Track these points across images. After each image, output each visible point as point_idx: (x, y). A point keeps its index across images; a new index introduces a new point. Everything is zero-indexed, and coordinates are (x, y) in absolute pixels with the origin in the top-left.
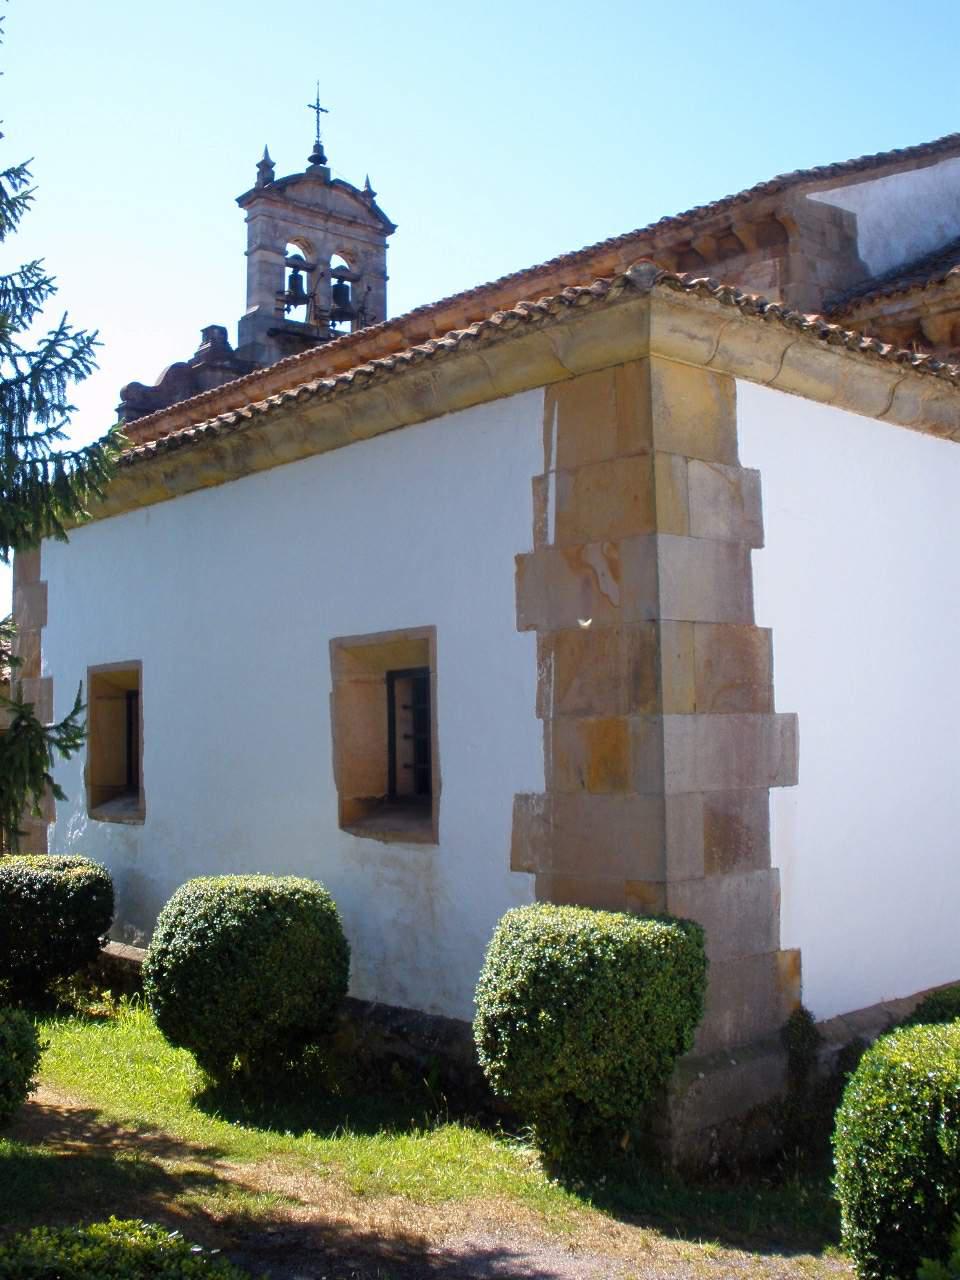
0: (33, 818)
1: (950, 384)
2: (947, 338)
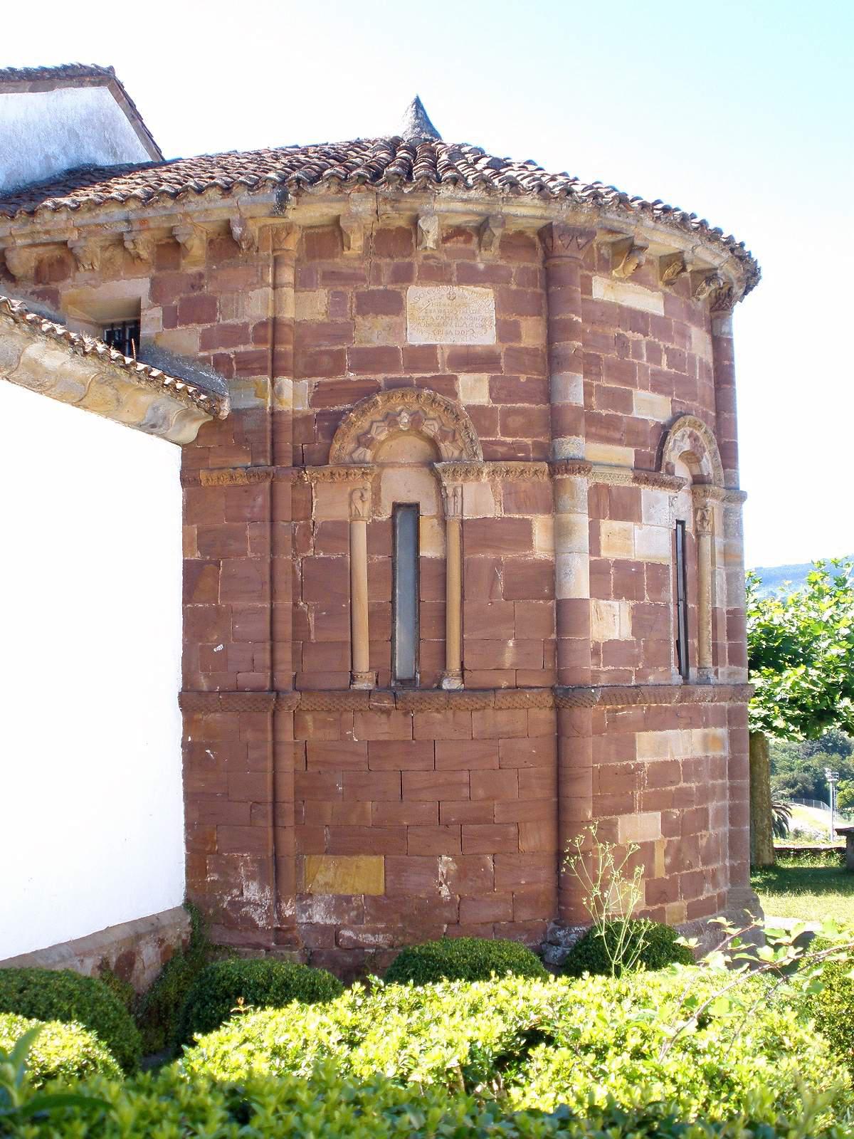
0: (824, 763)
1: (11, 320)
2: (31, 273)
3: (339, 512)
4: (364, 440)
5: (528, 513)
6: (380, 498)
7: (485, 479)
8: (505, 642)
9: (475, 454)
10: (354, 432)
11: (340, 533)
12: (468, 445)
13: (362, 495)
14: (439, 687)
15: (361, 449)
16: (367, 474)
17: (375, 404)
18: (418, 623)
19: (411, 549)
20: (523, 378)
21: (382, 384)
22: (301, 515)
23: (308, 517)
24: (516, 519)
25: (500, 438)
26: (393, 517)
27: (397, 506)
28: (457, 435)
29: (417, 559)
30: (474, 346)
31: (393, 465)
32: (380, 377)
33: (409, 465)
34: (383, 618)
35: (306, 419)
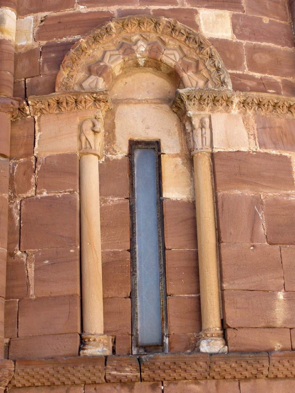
3: (68, 144)
4: (96, 69)
5: (285, 149)
6: (114, 136)
7: (235, 110)
8: (273, 294)
9: (223, 83)
10: (84, 60)
11: (69, 168)
12: (214, 74)
13: (94, 125)
14: (195, 348)
15: (93, 78)
16: (99, 100)
17: (108, 31)
18: (164, 274)
19: (153, 190)
20: (266, 20)
21: (116, 15)
22: (22, 152)
23: (28, 155)
24: (273, 155)
25: (247, 71)
26: (130, 155)
27: (134, 144)
28: (201, 66)
29: (160, 202)
31: (128, 101)
32: (114, 9)
33: (147, 101)
34: (121, 269)
35: (30, 53)
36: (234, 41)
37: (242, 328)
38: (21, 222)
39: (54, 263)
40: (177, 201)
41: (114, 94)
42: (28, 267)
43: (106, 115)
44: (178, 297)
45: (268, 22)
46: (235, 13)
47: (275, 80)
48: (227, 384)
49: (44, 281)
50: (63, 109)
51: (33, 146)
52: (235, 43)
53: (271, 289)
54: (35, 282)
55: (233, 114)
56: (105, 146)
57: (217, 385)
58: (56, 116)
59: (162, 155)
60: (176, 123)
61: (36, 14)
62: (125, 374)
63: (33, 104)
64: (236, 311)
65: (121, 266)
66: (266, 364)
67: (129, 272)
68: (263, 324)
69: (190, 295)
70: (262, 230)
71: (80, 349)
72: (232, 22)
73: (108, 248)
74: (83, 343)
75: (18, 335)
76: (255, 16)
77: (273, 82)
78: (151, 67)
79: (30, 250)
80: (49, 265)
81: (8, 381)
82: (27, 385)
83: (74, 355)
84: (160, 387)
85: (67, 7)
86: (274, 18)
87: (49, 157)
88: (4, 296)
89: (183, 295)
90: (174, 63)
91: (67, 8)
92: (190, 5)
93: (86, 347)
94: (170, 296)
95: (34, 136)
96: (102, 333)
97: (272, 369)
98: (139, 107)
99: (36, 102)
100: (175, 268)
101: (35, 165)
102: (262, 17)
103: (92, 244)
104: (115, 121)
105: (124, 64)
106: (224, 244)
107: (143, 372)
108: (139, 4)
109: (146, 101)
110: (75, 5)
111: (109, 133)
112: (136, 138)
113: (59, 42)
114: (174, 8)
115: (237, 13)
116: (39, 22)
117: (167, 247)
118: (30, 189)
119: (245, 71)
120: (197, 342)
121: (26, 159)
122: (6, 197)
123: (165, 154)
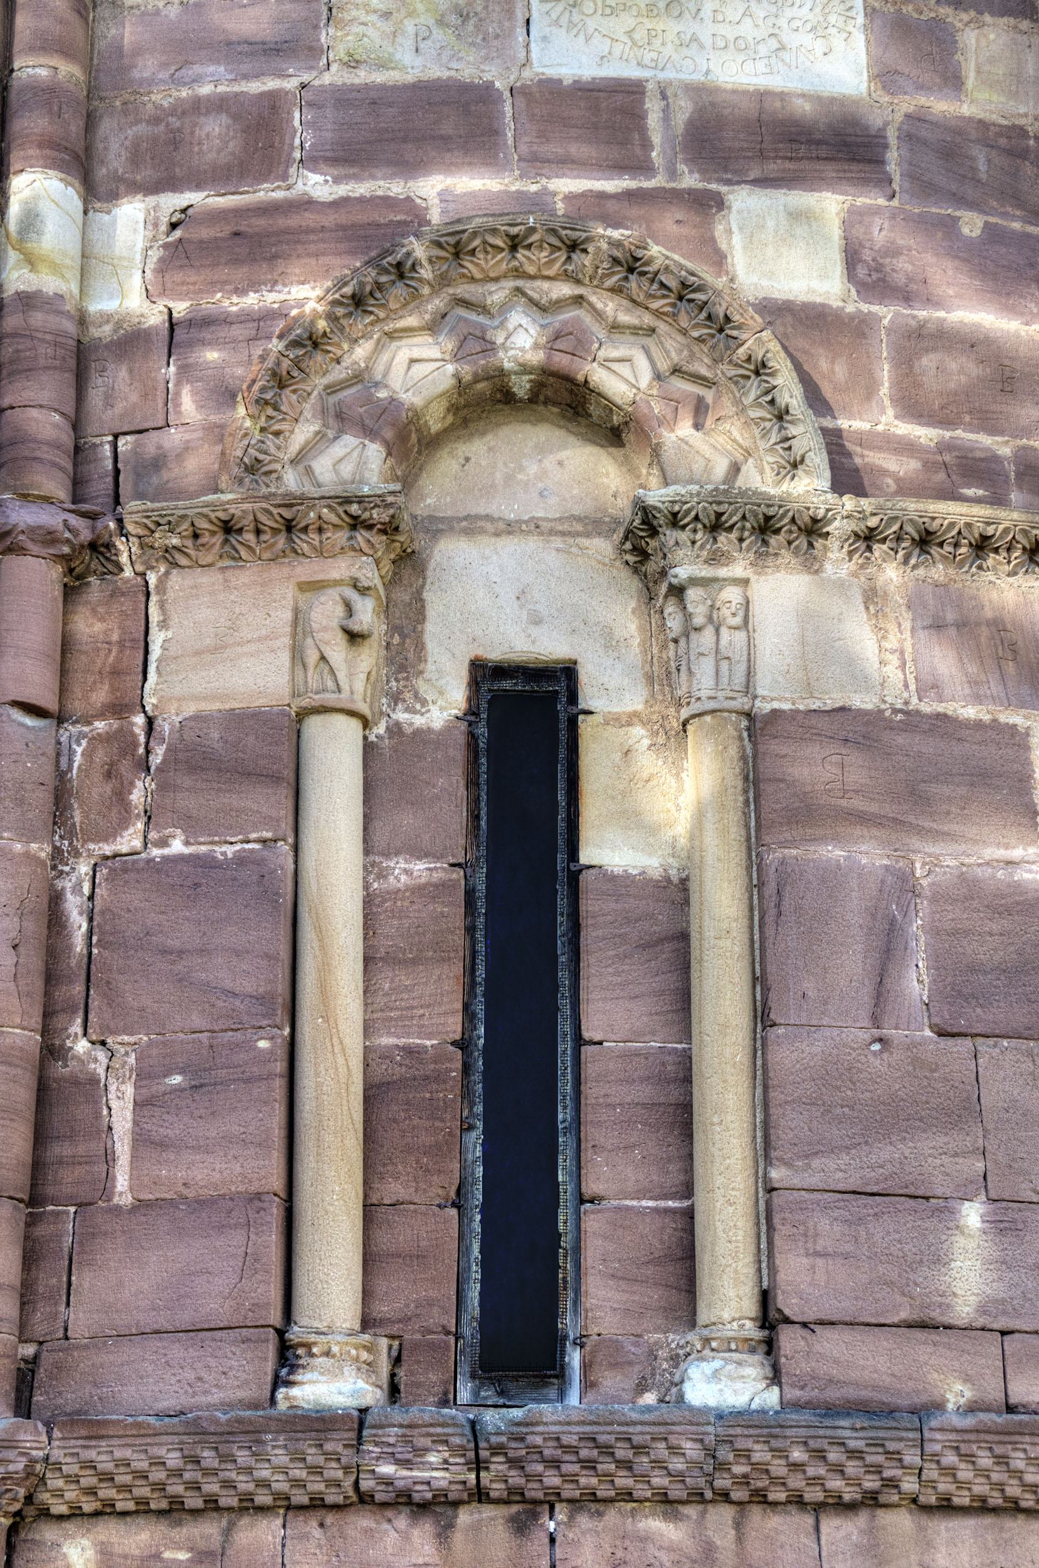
3: (259, 677)
6: (420, 646)
22: (101, 696)
24: (966, 724)
30: (782, 96)
31: (471, 526)
36: (850, 309)
37: (833, 1323)
38: (95, 939)
39: (201, 1086)
40: (627, 876)
41: (423, 499)
42: (112, 1096)
43: (395, 574)
44: (619, 1209)
45: (977, 233)
46: (861, 201)
47: (988, 449)
48: (775, 1521)
49: (162, 1145)
50: (244, 553)
51: (140, 677)
52: (852, 317)
53: (939, 1192)
54: (135, 1148)
55: (829, 580)
56: (388, 682)
57: (738, 1525)
58: (220, 577)
59: (581, 717)
60: (633, 604)
61: (152, 200)
62: (426, 1474)
63: (141, 531)
64: (813, 1267)
65: (428, 1095)
66: (912, 1457)
67: (454, 1118)
68: (904, 1315)
69: (662, 1204)
70: (916, 982)
71: (277, 1382)
72: (846, 238)
73: (389, 1034)
74: (288, 1358)
75: (66, 1330)
76: (934, 210)
77: (982, 460)
78: (556, 404)
79: (119, 1039)
80: (182, 1090)
81: (22, 1492)
82: (87, 1508)
83: (255, 1406)
84: (542, 1525)
85: (264, 175)
86: (1004, 215)
87: (197, 718)
88: (26, 1197)
89: (635, 1203)
90: (630, 394)
91: (265, 181)
92: (697, 176)
93: (298, 1378)
94: (592, 1202)
95: (142, 643)
96: (357, 1327)
97: (931, 1473)
98: (509, 548)
99: (152, 526)
100: (613, 1107)
101: (147, 743)
102: (958, 213)
103: (332, 1021)
104: (425, 595)
105: (460, 395)
106: (781, 1031)
107: (487, 1469)
108: (517, 173)
109: (532, 527)
110: (293, 170)
111: (404, 637)
112: (495, 654)
113: (234, 309)
114: (640, 189)
115: (868, 201)
116: (163, 228)
117: (586, 1035)
118: (127, 828)
119: (883, 419)
120: (676, 1366)
121: (116, 724)
122: (43, 855)
123: (591, 713)
